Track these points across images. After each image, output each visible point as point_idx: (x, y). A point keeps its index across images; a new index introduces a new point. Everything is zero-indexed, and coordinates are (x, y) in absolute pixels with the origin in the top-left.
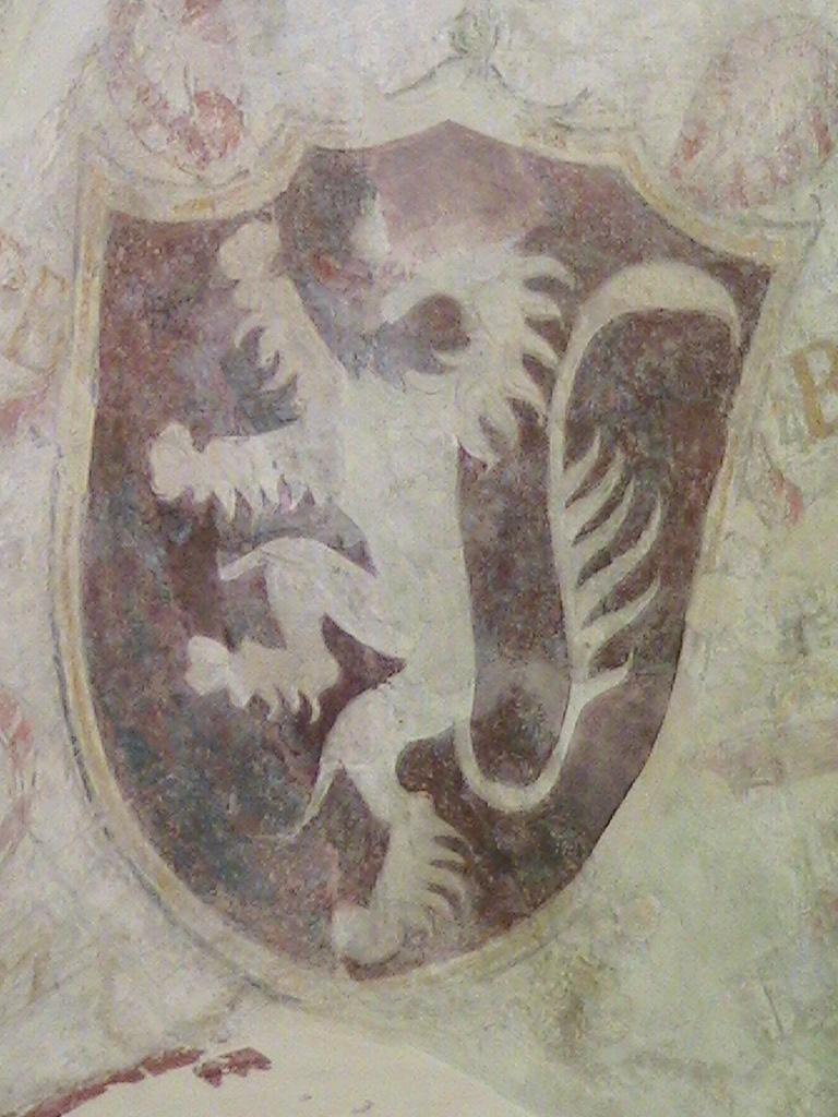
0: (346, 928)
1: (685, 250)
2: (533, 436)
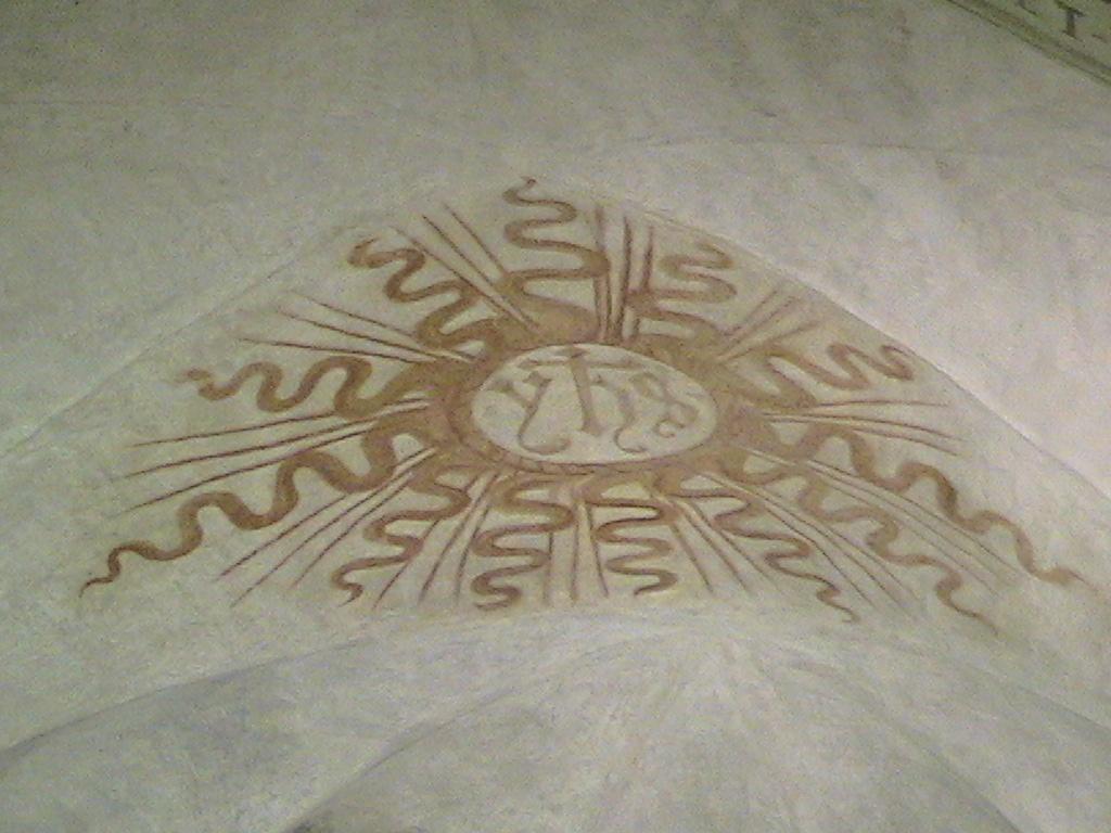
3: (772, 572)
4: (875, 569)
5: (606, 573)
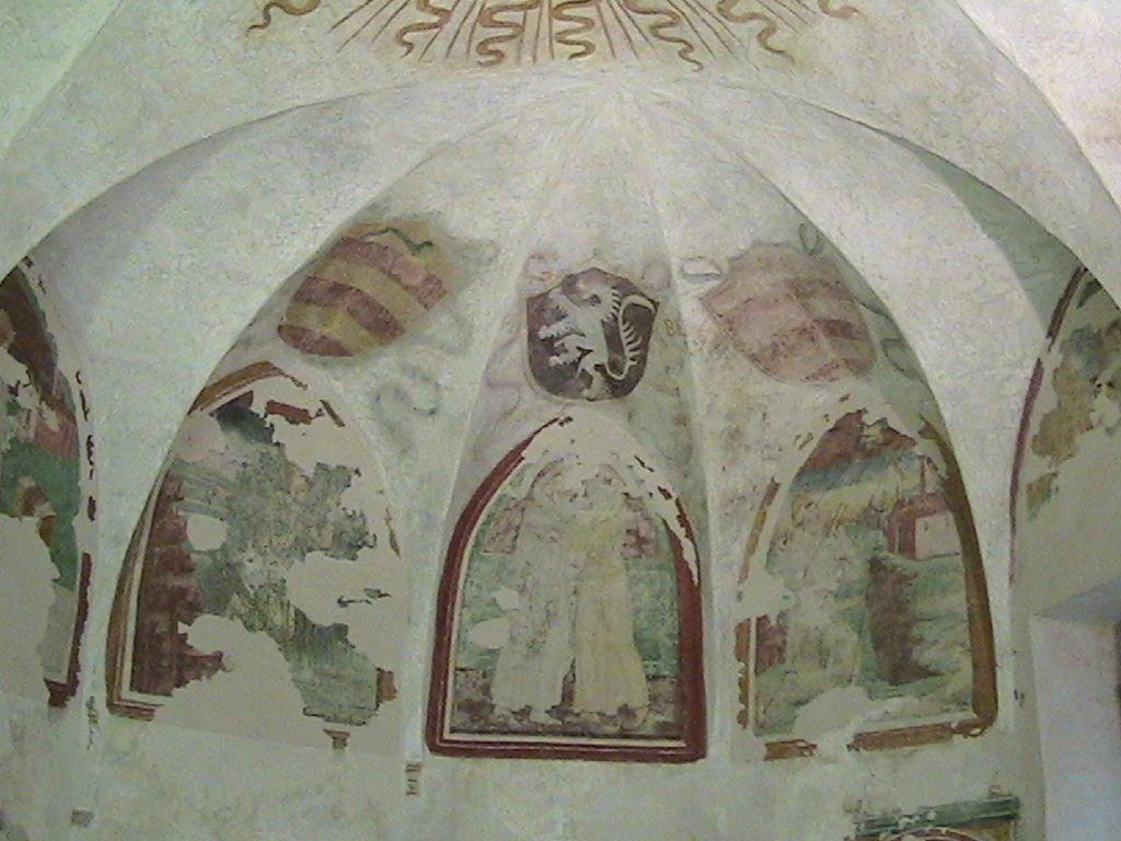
0: (586, 392)
1: (642, 295)
2: (616, 319)
3: (653, 39)
4: (718, 27)
5: (554, 42)
